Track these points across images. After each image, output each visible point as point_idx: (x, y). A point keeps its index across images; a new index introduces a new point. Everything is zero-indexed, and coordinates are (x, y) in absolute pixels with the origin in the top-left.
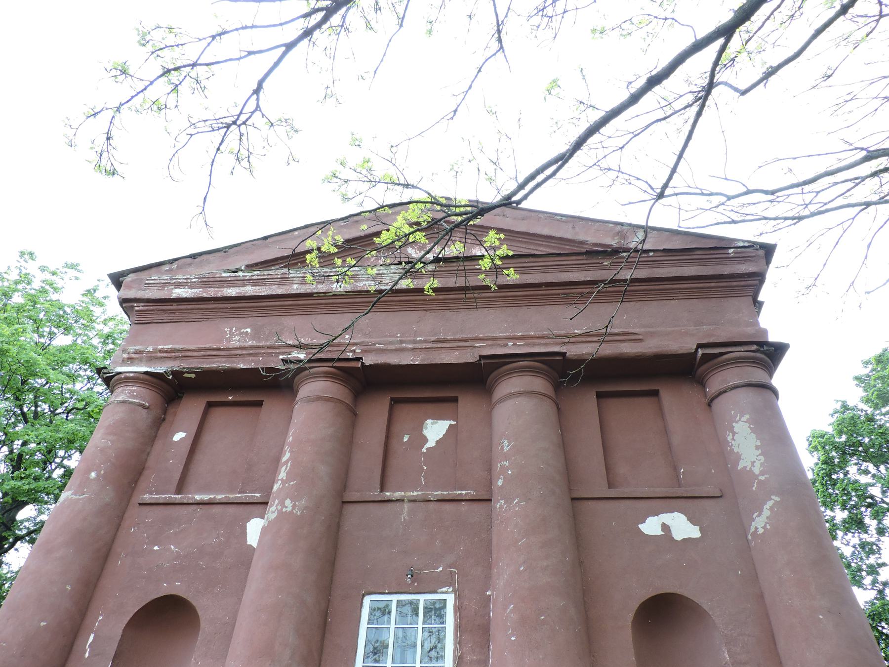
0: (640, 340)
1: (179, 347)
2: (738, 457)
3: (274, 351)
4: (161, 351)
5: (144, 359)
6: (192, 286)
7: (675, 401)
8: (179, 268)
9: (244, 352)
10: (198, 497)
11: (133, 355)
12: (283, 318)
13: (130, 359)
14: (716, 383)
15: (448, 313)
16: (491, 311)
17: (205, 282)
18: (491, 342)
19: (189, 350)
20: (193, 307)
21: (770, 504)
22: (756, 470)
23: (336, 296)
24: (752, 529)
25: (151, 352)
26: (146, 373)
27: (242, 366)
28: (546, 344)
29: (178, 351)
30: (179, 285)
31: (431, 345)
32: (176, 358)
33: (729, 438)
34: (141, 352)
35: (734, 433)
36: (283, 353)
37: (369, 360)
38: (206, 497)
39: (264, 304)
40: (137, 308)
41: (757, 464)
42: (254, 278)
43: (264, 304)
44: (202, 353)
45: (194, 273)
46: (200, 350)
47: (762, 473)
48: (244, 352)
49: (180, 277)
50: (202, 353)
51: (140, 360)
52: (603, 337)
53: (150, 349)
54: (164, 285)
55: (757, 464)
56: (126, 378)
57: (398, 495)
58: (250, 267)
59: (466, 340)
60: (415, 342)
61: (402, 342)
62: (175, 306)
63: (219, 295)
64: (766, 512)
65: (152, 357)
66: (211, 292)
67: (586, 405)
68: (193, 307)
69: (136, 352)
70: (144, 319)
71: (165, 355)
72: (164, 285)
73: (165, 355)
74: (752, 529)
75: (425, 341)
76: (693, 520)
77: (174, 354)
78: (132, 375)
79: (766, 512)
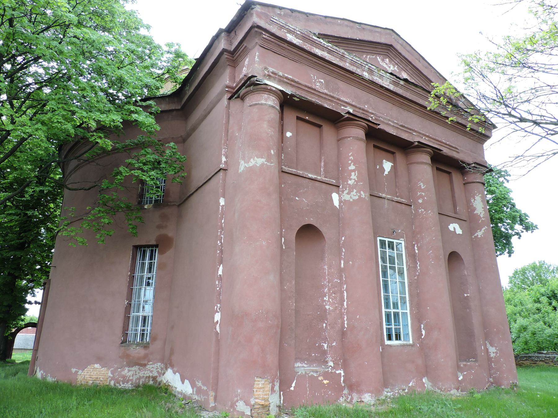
0: (458, 152)
1: (297, 80)
2: (475, 209)
3: (340, 102)
4: (287, 78)
5: (277, 79)
6: (297, 36)
7: (328, 131)
8: (285, 15)
9: (327, 97)
10: (310, 176)
11: (271, 74)
12: (337, 80)
13: (269, 75)
14: (470, 178)
15: (401, 110)
16: (415, 116)
17: (305, 38)
18: (418, 134)
19: (300, 84)
20: (295, 51)
21: (484, 229)
22: (482, 216)
23: (363, 79)
24: (476, 235)
25: (281, 76)
26: (281, 91)
27: (326, 106)
28: (434, 143)
29: (295, 82)
30: (290, 32)
31: (399, 127)
32: (293, 86)
33: (472, 201)
34: (275, 74)
35: (475, 200)
36: (344, 106)
37: (381, 127)
38: (314, 176)
39: (331, 68)
40: (264, 36)
41: (482, 214)
42: (329, 48)
43: (331, 68)
44: (306, 89)
45: (298, 26)
46: (306, 86)
47: (483, 217)
48: (327, 97)
49: (292, 27)
50: (306, 89)
51: (275, 78)
52: (450, 147)
53: (281, 74)
54: (282, 27)
55: (482, 214)
56: (271, 90)
57: (384, 195)
58: (321, 36)
59: (410, 129)
60: (394, 122)
61: (389, 120)
62: (285, 46)
63: (312, 51)
64: (483, 231)
65: (281, 80)
66: (307, 47)
67: (291, 117)
68: (295, 51)
69: (273, 73)
70: (266, 45)
71: (288, 81)
72: (282, 27)
73: (288, 81)
74: (476, 235)
75: (397, 124)
76: (461, 228)
77: (292, 83)
78: (274, 89)
79: (483, 231)
